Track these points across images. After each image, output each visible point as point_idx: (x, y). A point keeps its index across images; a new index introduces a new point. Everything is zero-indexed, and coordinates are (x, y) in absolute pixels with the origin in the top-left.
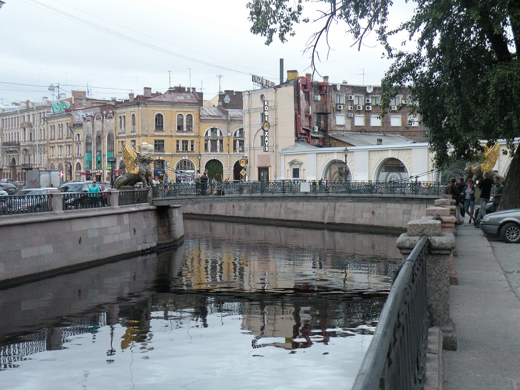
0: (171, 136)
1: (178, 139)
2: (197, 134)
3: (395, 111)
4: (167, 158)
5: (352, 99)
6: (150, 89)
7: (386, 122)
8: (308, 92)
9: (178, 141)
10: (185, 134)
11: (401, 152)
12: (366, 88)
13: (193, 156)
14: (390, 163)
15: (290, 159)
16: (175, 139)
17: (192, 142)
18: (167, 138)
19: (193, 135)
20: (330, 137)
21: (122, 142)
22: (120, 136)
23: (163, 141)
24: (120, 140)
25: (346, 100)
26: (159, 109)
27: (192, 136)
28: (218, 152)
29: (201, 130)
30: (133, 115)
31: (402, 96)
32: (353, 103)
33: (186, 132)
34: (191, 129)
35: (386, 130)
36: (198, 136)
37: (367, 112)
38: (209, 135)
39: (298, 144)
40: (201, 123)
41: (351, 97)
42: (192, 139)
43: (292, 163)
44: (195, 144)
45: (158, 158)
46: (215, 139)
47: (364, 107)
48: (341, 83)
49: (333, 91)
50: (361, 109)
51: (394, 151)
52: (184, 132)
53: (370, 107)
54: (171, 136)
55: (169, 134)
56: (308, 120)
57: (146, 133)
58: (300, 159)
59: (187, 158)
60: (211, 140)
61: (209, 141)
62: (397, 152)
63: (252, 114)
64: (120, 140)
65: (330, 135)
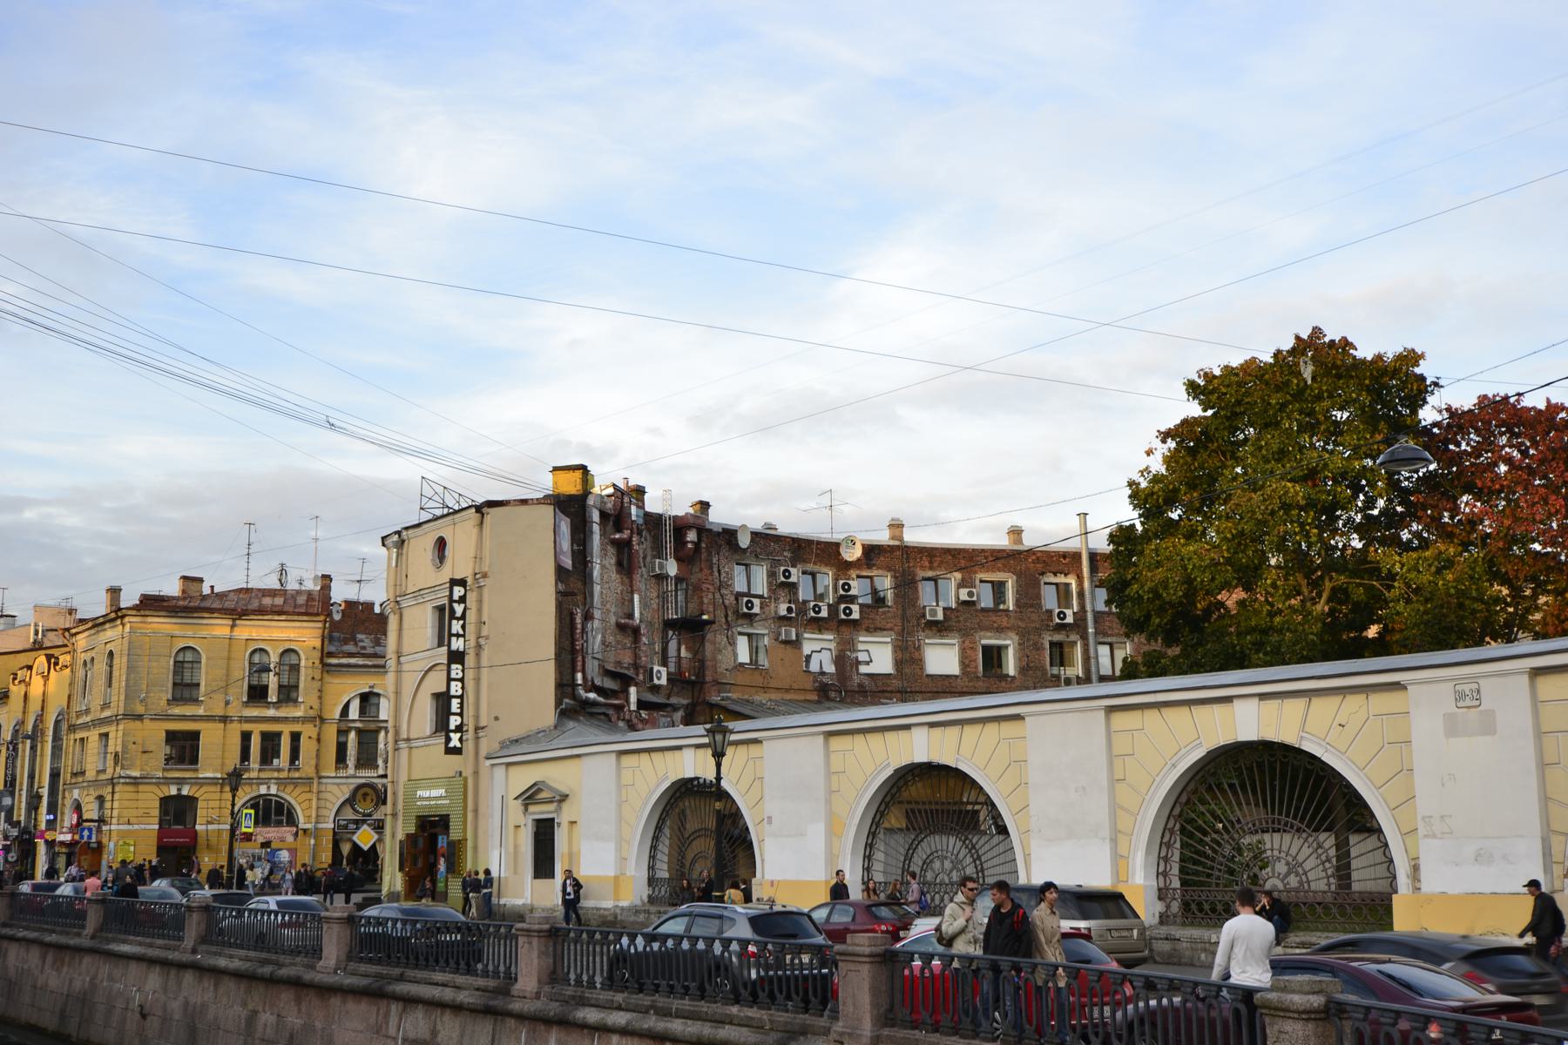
0: (225, 719)
1: (247, 727)
2: (312, 713)
3: (937, 622)
4: (204, 789)
5: (793, 579)
6: (201, 580)
7: (908, 658)
8: (629, 542)
9: (246, 736)
10: (271, 712)
11: (971, 732)
12: (837, 545)
13: (295, 782)
14: (917, 790)
15: (523, 779)
16: (235, 729)
17: (296, 737)
18: (210, 725)
19: (299, 714)
20: (712, 706)
21: (82, 740)
22: (80, 721)
23: (195, 736)
24: (79, 735)
25: (770, 584)
26: (190, 633)
27: (295, 720)
28: (351, 771)
29: (327, 699)
30: (111, 654)
31: (958, 575)
32: (796, 593)
33: (277, 705)
34: (294, 695)
35: (910, 682)
36: (321, 719)
37: (839, 624)
38: (354, 713)
39: (571, 724)
40: (327, 678)
41: (787, 574)
42: (296, 728)
43: (530, 797)
44: (307, 747)
45: (173, 791)
46: (372, 726)
47: (833, 609)
48: (758, 526)
49: (725, 551)
50: (824, 613)
51: (937, 731)
52: (268, 705)
53: (855, 608)
54: (225, 719)
55: (219, 712)
56: (628, 642)
57: (140, 709)
58: (557, 776)
59: (273, 790)
60: (359, 731)
61: (352, 735)
62: (953, 732)
63: (406, 613)
64: (79, 735)
65: (715, 699)
